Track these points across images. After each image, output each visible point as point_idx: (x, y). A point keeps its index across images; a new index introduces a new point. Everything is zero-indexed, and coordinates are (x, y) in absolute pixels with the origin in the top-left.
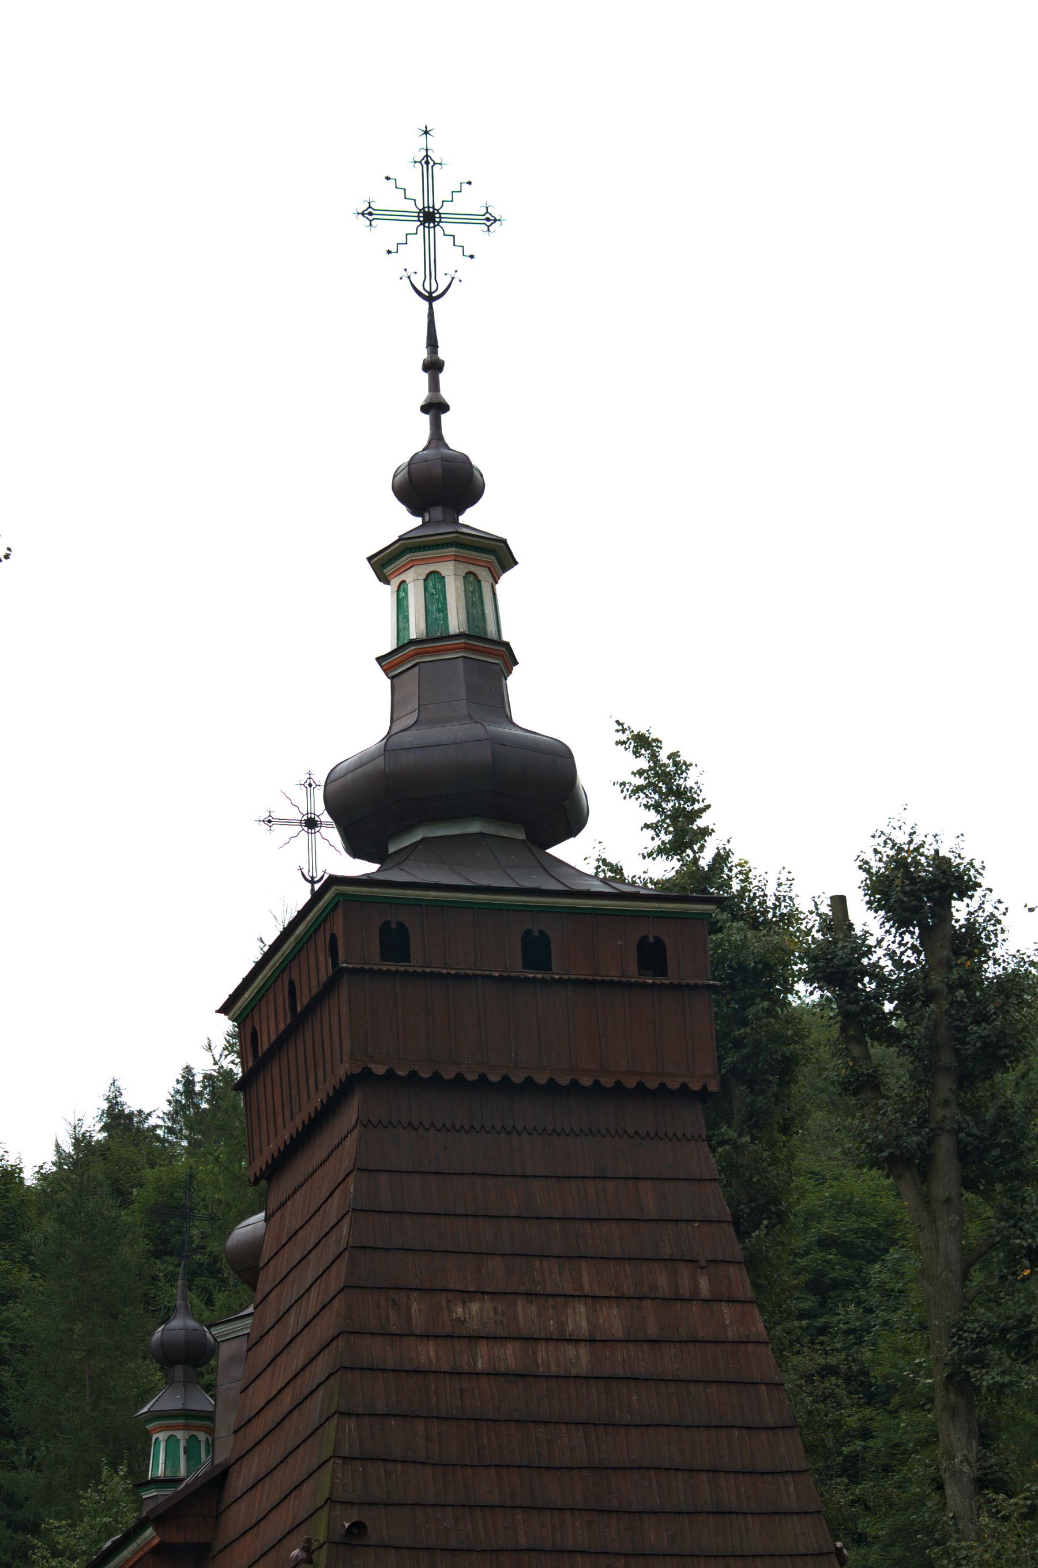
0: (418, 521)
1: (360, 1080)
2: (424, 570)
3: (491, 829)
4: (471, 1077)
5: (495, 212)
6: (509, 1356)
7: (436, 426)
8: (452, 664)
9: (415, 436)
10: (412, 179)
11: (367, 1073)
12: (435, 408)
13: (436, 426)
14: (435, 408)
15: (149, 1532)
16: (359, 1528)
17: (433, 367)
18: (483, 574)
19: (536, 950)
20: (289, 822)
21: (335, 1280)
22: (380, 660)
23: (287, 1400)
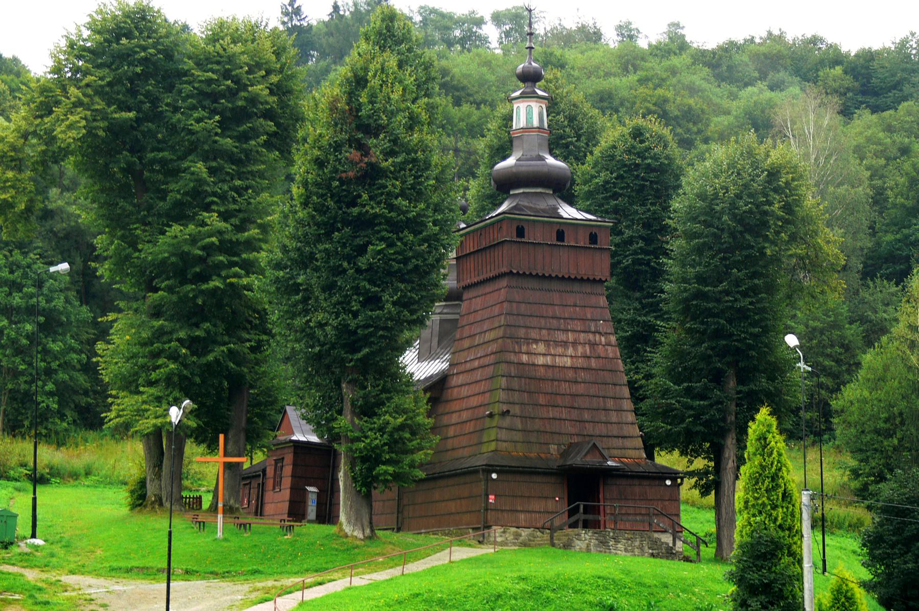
2: (526, 104)
11: (511, 272)
16: (508, 411)
23: (476, 364)
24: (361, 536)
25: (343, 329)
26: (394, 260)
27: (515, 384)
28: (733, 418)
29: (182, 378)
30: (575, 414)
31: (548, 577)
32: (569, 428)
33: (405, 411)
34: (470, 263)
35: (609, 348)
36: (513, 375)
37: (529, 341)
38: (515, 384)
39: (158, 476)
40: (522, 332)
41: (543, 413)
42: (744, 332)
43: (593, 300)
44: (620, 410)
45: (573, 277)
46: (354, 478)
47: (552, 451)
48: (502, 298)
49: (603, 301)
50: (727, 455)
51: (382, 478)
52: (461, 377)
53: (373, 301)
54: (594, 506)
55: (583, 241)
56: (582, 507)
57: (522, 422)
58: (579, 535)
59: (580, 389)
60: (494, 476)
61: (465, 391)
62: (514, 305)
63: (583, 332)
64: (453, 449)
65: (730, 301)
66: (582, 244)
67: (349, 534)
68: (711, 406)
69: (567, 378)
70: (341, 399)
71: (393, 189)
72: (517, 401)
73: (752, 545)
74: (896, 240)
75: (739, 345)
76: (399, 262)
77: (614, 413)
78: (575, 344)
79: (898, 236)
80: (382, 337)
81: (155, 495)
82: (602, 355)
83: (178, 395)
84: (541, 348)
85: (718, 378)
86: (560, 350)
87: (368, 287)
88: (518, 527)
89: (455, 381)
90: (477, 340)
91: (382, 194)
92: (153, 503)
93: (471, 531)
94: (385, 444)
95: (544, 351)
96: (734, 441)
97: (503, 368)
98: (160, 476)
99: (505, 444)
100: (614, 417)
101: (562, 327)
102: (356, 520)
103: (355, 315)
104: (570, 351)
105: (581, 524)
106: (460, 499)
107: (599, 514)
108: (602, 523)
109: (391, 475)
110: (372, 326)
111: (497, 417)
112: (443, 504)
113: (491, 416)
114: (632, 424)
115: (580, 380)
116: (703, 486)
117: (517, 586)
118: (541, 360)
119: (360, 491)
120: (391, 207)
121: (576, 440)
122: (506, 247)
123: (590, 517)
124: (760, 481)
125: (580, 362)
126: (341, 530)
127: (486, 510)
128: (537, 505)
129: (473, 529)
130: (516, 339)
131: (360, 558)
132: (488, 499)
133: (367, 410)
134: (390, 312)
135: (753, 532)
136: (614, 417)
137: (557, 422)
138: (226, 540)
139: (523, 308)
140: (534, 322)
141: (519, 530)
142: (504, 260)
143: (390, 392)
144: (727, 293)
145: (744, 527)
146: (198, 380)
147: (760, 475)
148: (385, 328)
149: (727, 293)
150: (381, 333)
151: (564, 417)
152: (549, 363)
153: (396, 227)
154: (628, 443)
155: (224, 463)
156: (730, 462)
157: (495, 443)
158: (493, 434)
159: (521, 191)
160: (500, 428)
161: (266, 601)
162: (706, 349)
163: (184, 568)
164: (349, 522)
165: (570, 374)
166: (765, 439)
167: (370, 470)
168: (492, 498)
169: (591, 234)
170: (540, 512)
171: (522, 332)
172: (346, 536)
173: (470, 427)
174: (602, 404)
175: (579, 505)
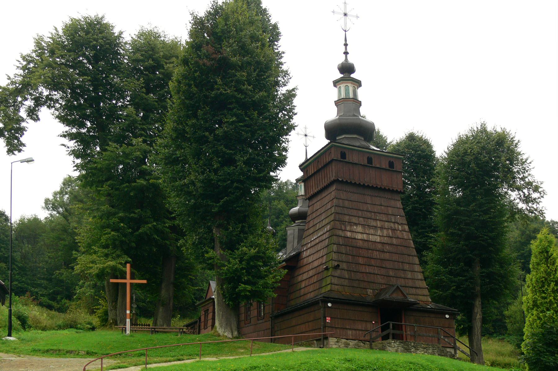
0: (342, 76)
1: (336, 181)
2: (345, 85)
3: (357, 137)
4: (357, 183)
5: (358, 15)
6: (365, 237)
7: (346, 57)
8: (349, 103)
9: (341, 59)
10: (342, 6)
11: (338, 179)
12: (346, 53)
13: (346, 57)
14: (346, 53)
15: (284, 263)
16: (338, 266)
17: (346, 45)
18: (356, 87)
19: (370, 160)
20: (302, 135)
21: (332, 218)
23: (317, 241)
24: (230, 336)
25: (208, 183)
26: (243, 131)
27: (343, 249)
28: (479, 288)
29: (122, 242)
30: (383, 271)
31: (369, 360)
32: (380, 280)
33: (258, 245)
34: (312, 182)
35: (404, 233)
36: (341, 244)
37: (351, 223)
38: (343, 249)
39: (115, 308)
40: (347, 218)
41: (363, 269)
42: (486, 236)
43: (392, 203)
44: (413, 271)
46: (224, 295)
47: (369, 293)
48: (333, 197)
49: (399, 204)
50: (476, 311)
51: (243, 294)
52: (309, 251)
53: (230, 161)
54: (399, 325)
55: (385, 165)
56: (391, 325)
57: (348, 273)
58: (390, 343)
59: (387, 256)
60: (330, 305)
61: (310, 259)
62: (341, 201)
63: (387, 221)
64: (304, 295)
65: (477, 216)
66: (384, 167)
67: (221, 334)
68: (466, 280)
69: (378, 249)
70: (213, 240)
71: (240, 78)
72: (344, 260)
73: (543, 334)
74: (518, 255)
75: (483, 243)
76: (247, 132)
77: (410, 273)
78: (382, 228)
79: (519, 254)
80: (237, 188)
81: (112, 319)
82: (400, 237)
83: (119, 253)
84: (360, 229)
85: (469, 263)
86: (372, 231)
87: (224, 149)
88: (347, 339)
89: (305, 254)
90: (318, 227)
91: (232, 81)
92: (111, 324)
93: (315, 342)
94: (243, 269)
95: (361, 231)
96: (480, 303)
97: (335, 239)
98: (116, 308)
99: (336, 287)
100: (409, 275)
101: (373, 217)
102: (227, 325)
103: (216, 171)
104: (379, 232)
105: (391, 337)
106: (308, 322)
107: (402, 330)
108: (404, 335)
109: (249, 291)
110: (229, 180)
111: (331, 270)
112: (298, 327)
113: (327, 269)
114: (421, 280)
115: (386, 251)
116: (461, 330)
117: (344, 365)
118: (359, 236)
119: (228, 305)
120: (240, 91)
121: (384, 286)
122: (334, 163)
123: (398, 332)
124: (546, 283)
125: (386, 240)
126: (216, 331)
127: (325, 327)
128: (360, 326)
129: (317, 340)
130: (342, 222)
131: (226, 349)
132: (326, 320)
133: (231, 246)
134: (241, 169)
135: (542, 324)
136: (409, 275)
137: (372, 275)
138: (131, 336)
139: (347, 203)
140: (354, 212)
141: (348, 341)
142: (332, 173)
143: (247, 234)
144: (474, 211)
145: (534, 321)
146: (133, 245)
147: (546, 279)
148: (239, 181)
149: (474, 211)
150: (235, 184)
151: (376, 273)
152: (365, 238)
153: (244, 106)
154: (419, 292)
155: (126, 279)
156: (478, 315)
157: (331, 285)
158: (328, 280)
159: (343, 136)
160: (333, 276)
161: (120, 368)
162: (463, 246)
163: (86, 350)
164: (221, 326)
165: (379, 246)
166: (547, 252)
167: (235, 288)
168: (328, 320)
169: (390, 161)
170: (362, 330)
171: (347, 218)
172: (219, 335)
173: (315, 279)
174: (401, 266)
175: (389, 324)
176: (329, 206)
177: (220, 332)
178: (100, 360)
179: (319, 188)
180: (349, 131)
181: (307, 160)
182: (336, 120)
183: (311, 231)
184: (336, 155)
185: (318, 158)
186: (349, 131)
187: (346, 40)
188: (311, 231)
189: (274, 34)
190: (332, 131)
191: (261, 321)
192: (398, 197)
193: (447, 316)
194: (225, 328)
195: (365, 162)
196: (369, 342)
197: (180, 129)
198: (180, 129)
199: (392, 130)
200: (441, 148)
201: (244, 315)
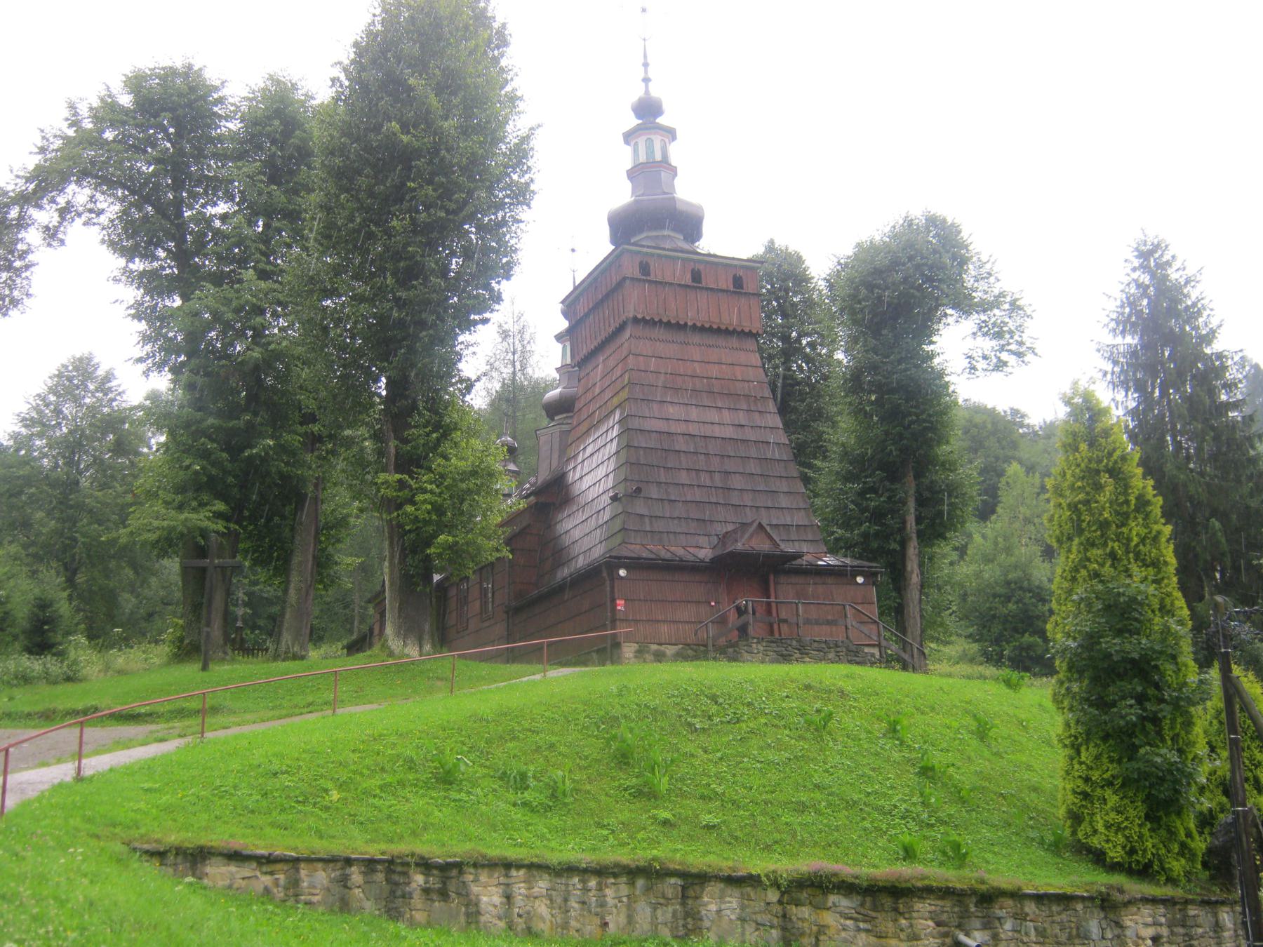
2: (644, 138)
7: (647, 87)
8: (651, 171)
9: (637, 93)
12: (646, 80)
13: (647, 87)
14: (646, 80)
16: (639, 490)
17: (646, 65)
22: (772, 242)
29: (211, 478)
43: (742, 357)
45: (715, 327)
48: (625, 353)
49: (755, 359)
60: (622, 573)
66: (724, 287)
67: (397, 652)
88: (660, 644)
129: (598, 651)
141: (662, 648)
168: (775, 304)
176: (618, 372)
177: (393, 647)
178: (77, 731)
179: (599, 340)
180: (653, 227)
181: (576, 288)
182: (629, 205)
183: (583, 428)
184: (631, 269)
185: (595, 279)
186: (653, 227)
187: (645, 56)
188: (583, 428)
189: (522, 195)
190: (625, 226)
191: (487, 624)
192: (750, 344)
193: (860, 580)
194: (405, 638)
195: (688, 279)
196: (696, 651)
197: (323, 236)
198: (323, 236)
199: (728, 237)
200: (820, 266)
201: (454, 614)
